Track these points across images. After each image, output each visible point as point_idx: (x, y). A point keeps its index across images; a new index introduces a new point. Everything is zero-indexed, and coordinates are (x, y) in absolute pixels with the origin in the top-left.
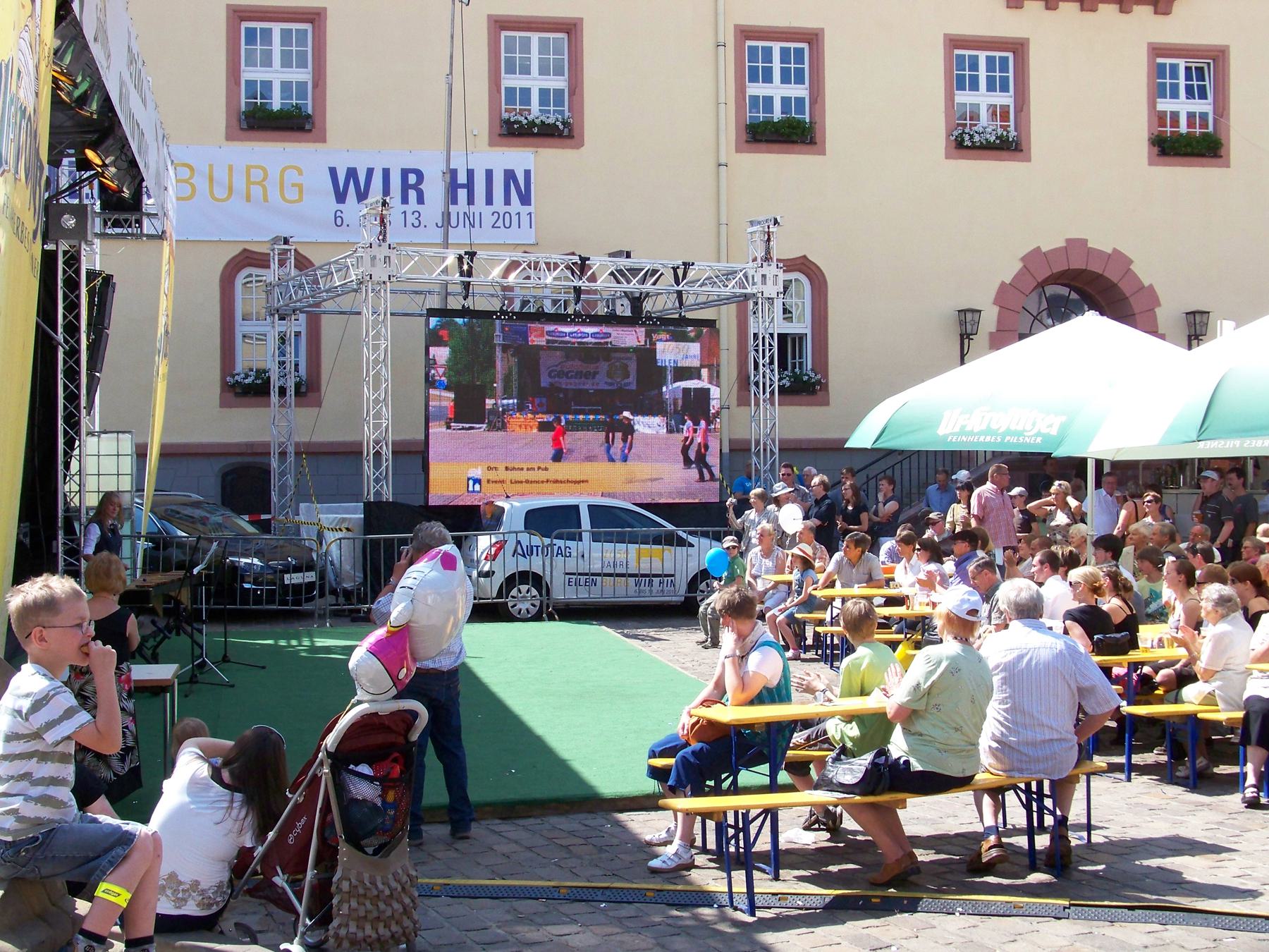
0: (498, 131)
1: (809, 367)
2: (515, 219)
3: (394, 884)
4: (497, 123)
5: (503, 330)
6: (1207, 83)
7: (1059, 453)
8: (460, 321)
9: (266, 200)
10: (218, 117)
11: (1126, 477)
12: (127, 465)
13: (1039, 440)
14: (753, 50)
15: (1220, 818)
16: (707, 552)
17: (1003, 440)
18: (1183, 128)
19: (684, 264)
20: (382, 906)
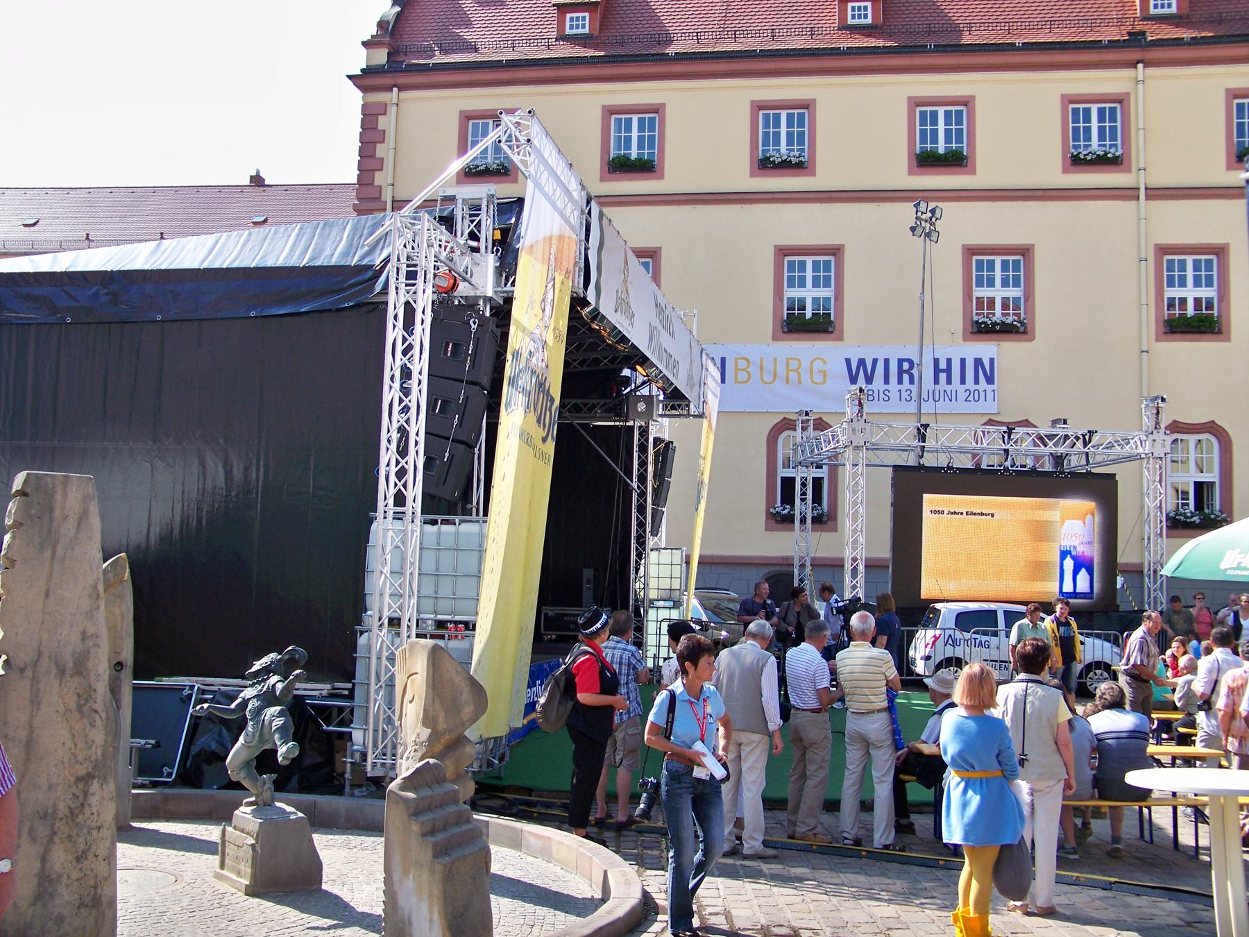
0: (970, 329)
2: (982, 394)
9: (800, 382)
10: (766, 322)
12: (677, 571)
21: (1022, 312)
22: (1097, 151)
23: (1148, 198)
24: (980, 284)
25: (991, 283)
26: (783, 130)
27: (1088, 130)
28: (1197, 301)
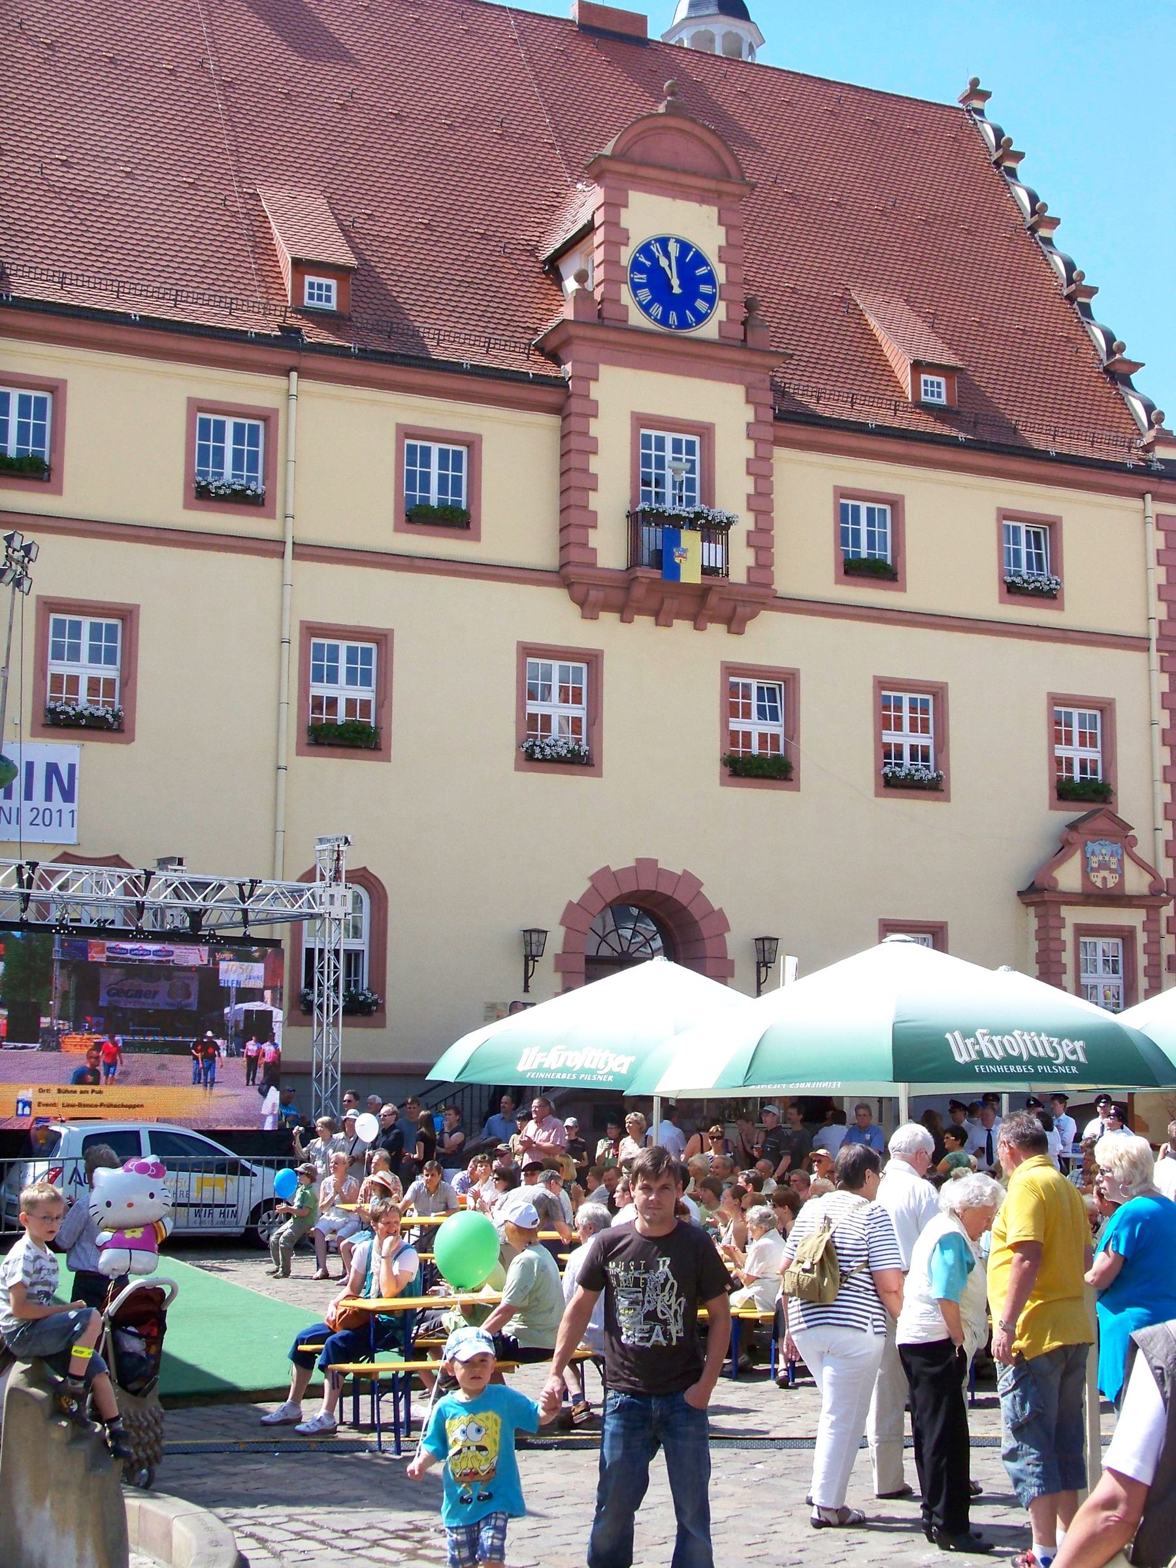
0: (42, 720)
1: (366, 986)
2: (56, 816)
3: (150, 1418)
4: (41, 712)
5: (62, 946)
6: (778, 704)
7: (630, 1092)
8: (17, 934)
11: (687, 1113)
13: (610, 1078)
14: (319, 648)
15: (753, 1394)
16: (269, 1180)
17: (577, 1077)
18: (755, 750)
19: (251, 881)
20: (142, 1433)
21: (117, 700)
22: (232, 483)
23: (296, 556)
24: (58, 656)
25: (75, 654)
26: (229, 446)
27: (219, 452)
28: (350, 703)
